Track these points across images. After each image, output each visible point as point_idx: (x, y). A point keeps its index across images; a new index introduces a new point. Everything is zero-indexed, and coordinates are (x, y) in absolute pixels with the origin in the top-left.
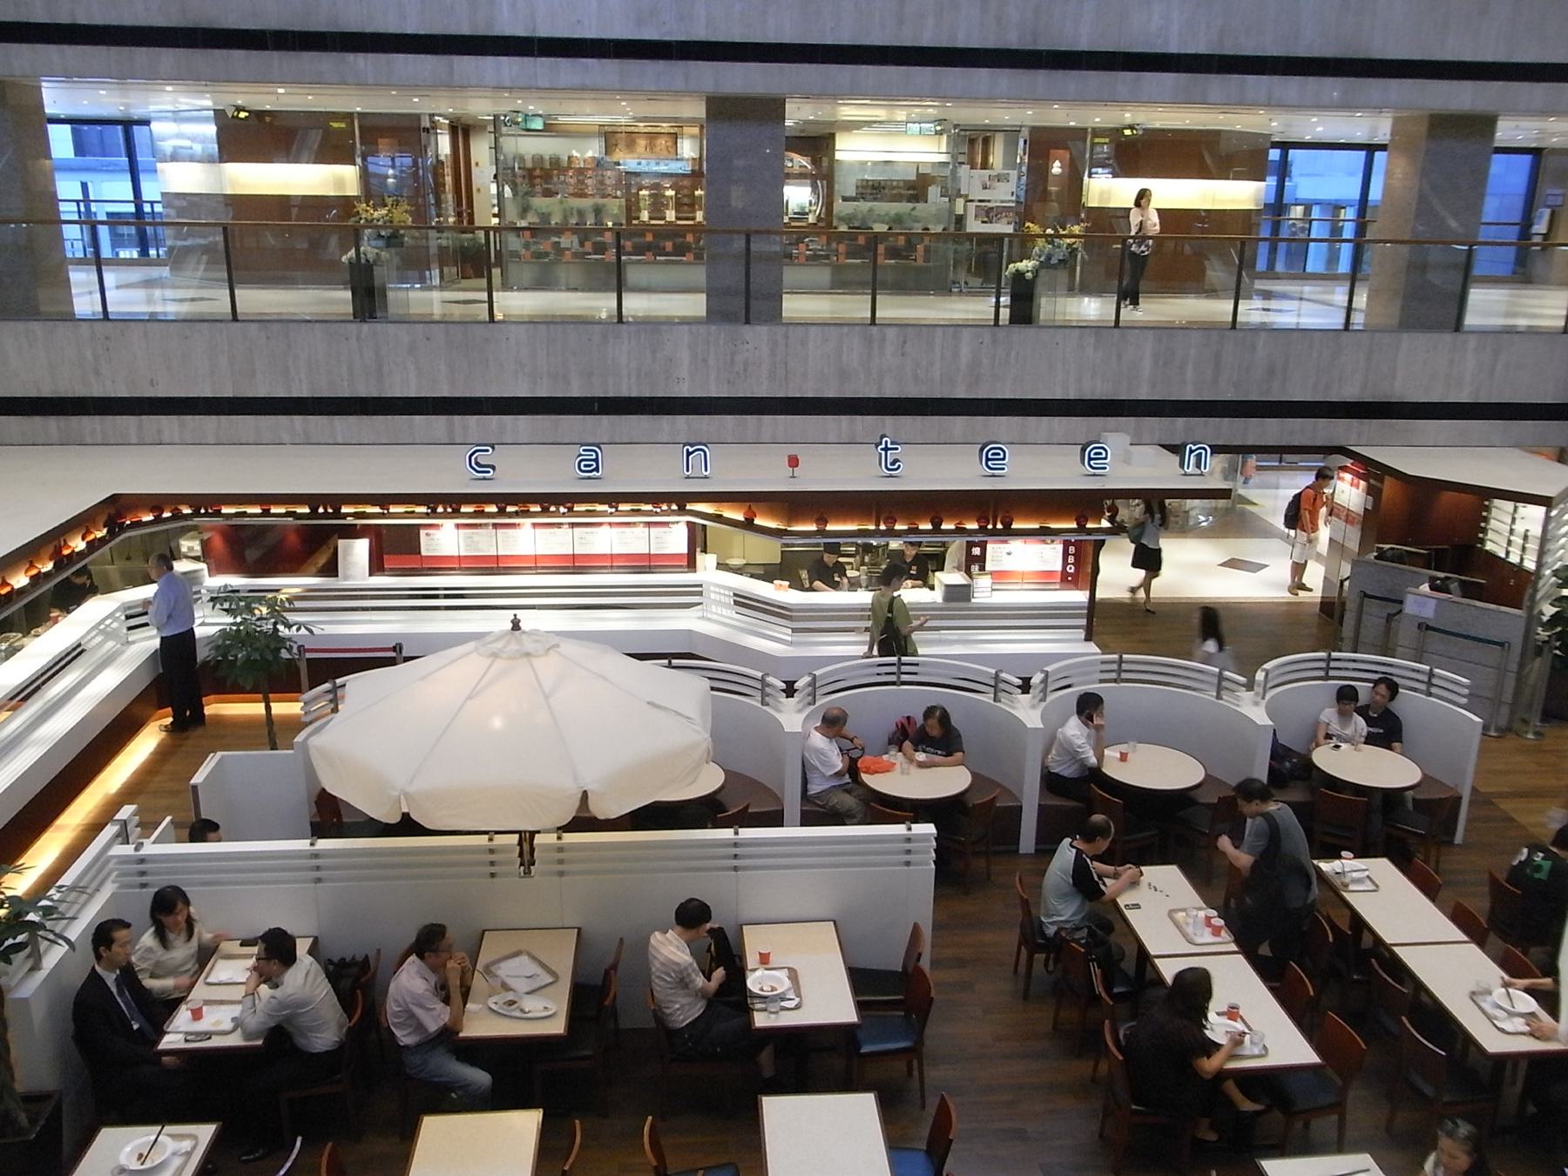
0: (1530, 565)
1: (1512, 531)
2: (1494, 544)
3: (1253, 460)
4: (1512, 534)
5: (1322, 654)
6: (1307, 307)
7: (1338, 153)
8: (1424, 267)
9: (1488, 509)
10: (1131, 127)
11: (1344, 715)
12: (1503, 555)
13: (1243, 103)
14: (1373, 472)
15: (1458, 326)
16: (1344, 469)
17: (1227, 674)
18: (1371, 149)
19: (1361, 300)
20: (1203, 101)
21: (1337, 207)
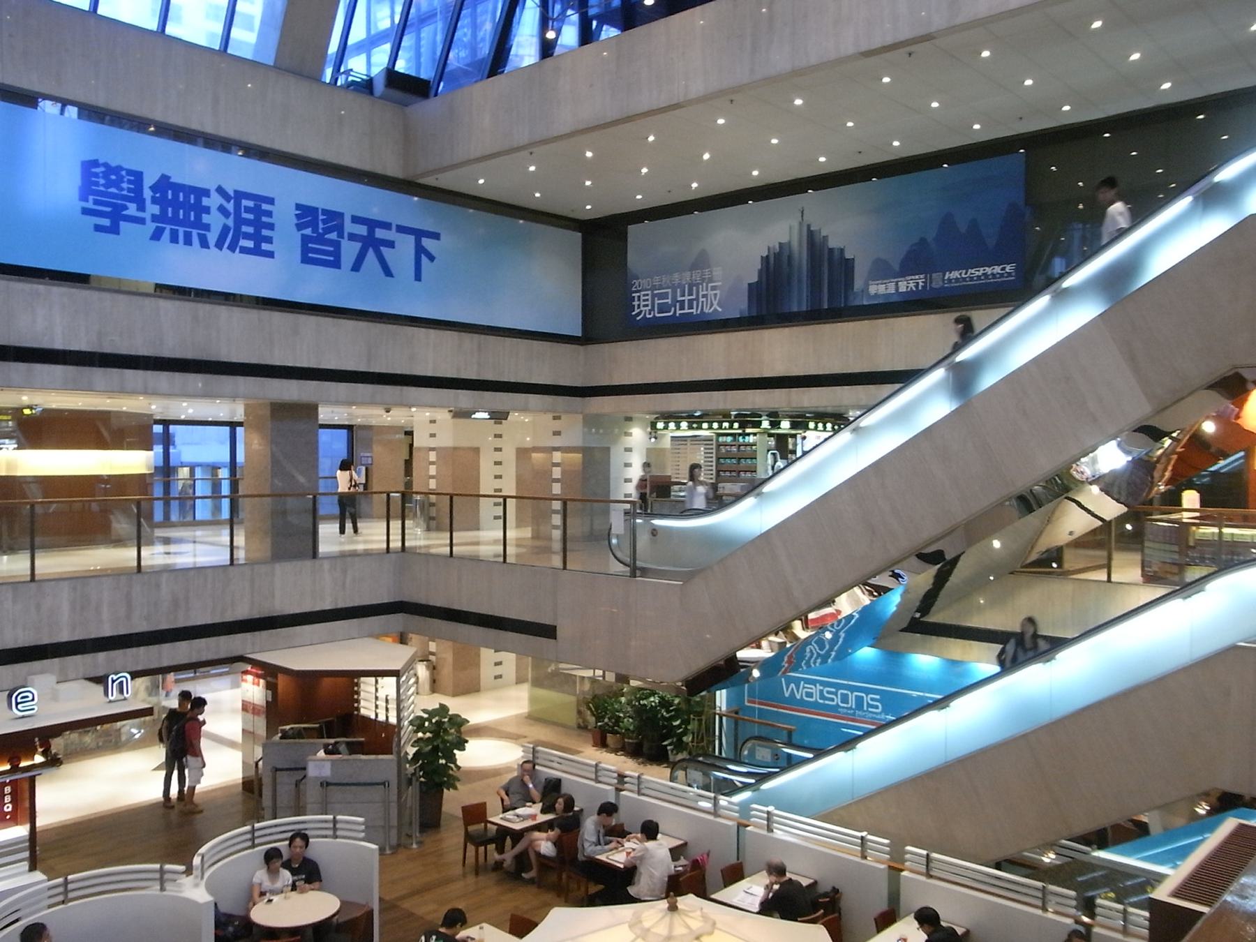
0: (393, 720)
1: (377, 698)
2: (367, 709)
3: (171, 677)
4: (376, 700)
5: (248, 828)
6: (200, 549)
7: (207, 432)
8: (284, 513)
9: (357, 685)
10: (31, 408)
11: (273, 873)
12: (373, 717)
13: (123, 391)
14: (269, 673)
15: (314, 554)
16: (246, 672)
17: (339, 817)
18: (233, 425)
19: (240, 540)
20: (89, 388)
21: (214, 468)
